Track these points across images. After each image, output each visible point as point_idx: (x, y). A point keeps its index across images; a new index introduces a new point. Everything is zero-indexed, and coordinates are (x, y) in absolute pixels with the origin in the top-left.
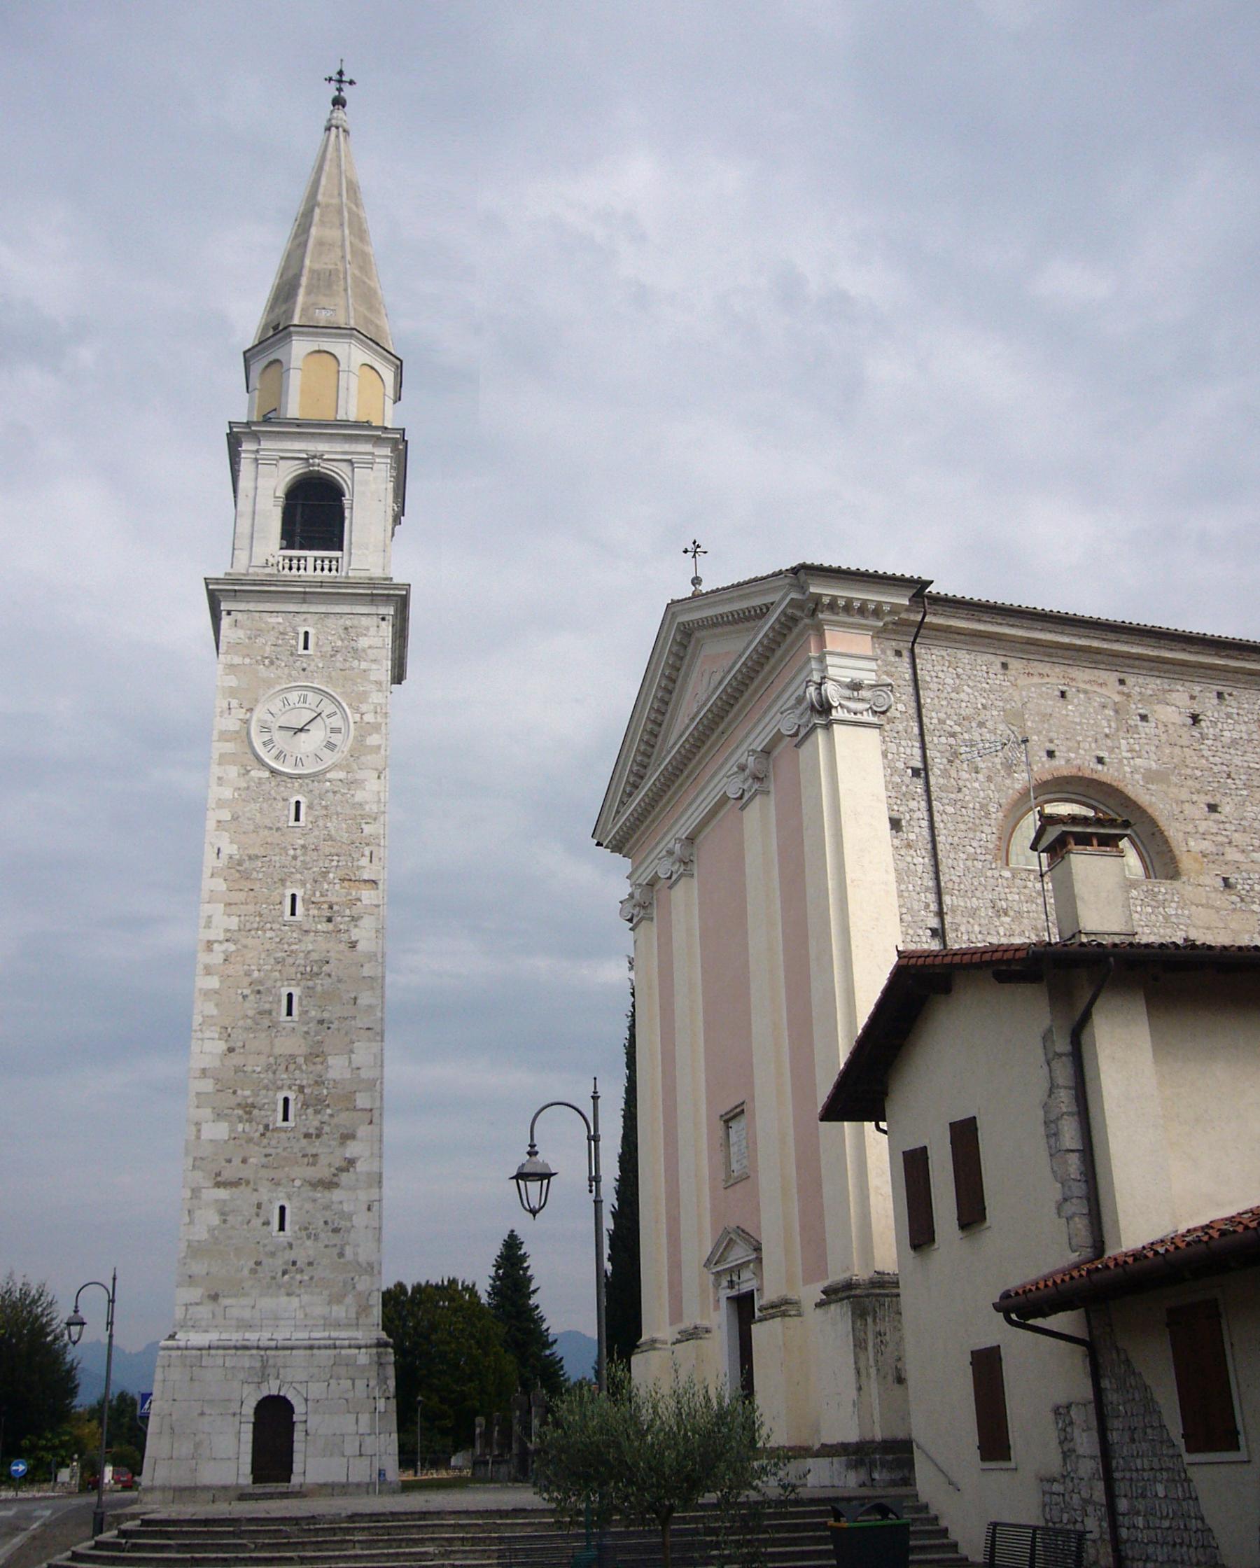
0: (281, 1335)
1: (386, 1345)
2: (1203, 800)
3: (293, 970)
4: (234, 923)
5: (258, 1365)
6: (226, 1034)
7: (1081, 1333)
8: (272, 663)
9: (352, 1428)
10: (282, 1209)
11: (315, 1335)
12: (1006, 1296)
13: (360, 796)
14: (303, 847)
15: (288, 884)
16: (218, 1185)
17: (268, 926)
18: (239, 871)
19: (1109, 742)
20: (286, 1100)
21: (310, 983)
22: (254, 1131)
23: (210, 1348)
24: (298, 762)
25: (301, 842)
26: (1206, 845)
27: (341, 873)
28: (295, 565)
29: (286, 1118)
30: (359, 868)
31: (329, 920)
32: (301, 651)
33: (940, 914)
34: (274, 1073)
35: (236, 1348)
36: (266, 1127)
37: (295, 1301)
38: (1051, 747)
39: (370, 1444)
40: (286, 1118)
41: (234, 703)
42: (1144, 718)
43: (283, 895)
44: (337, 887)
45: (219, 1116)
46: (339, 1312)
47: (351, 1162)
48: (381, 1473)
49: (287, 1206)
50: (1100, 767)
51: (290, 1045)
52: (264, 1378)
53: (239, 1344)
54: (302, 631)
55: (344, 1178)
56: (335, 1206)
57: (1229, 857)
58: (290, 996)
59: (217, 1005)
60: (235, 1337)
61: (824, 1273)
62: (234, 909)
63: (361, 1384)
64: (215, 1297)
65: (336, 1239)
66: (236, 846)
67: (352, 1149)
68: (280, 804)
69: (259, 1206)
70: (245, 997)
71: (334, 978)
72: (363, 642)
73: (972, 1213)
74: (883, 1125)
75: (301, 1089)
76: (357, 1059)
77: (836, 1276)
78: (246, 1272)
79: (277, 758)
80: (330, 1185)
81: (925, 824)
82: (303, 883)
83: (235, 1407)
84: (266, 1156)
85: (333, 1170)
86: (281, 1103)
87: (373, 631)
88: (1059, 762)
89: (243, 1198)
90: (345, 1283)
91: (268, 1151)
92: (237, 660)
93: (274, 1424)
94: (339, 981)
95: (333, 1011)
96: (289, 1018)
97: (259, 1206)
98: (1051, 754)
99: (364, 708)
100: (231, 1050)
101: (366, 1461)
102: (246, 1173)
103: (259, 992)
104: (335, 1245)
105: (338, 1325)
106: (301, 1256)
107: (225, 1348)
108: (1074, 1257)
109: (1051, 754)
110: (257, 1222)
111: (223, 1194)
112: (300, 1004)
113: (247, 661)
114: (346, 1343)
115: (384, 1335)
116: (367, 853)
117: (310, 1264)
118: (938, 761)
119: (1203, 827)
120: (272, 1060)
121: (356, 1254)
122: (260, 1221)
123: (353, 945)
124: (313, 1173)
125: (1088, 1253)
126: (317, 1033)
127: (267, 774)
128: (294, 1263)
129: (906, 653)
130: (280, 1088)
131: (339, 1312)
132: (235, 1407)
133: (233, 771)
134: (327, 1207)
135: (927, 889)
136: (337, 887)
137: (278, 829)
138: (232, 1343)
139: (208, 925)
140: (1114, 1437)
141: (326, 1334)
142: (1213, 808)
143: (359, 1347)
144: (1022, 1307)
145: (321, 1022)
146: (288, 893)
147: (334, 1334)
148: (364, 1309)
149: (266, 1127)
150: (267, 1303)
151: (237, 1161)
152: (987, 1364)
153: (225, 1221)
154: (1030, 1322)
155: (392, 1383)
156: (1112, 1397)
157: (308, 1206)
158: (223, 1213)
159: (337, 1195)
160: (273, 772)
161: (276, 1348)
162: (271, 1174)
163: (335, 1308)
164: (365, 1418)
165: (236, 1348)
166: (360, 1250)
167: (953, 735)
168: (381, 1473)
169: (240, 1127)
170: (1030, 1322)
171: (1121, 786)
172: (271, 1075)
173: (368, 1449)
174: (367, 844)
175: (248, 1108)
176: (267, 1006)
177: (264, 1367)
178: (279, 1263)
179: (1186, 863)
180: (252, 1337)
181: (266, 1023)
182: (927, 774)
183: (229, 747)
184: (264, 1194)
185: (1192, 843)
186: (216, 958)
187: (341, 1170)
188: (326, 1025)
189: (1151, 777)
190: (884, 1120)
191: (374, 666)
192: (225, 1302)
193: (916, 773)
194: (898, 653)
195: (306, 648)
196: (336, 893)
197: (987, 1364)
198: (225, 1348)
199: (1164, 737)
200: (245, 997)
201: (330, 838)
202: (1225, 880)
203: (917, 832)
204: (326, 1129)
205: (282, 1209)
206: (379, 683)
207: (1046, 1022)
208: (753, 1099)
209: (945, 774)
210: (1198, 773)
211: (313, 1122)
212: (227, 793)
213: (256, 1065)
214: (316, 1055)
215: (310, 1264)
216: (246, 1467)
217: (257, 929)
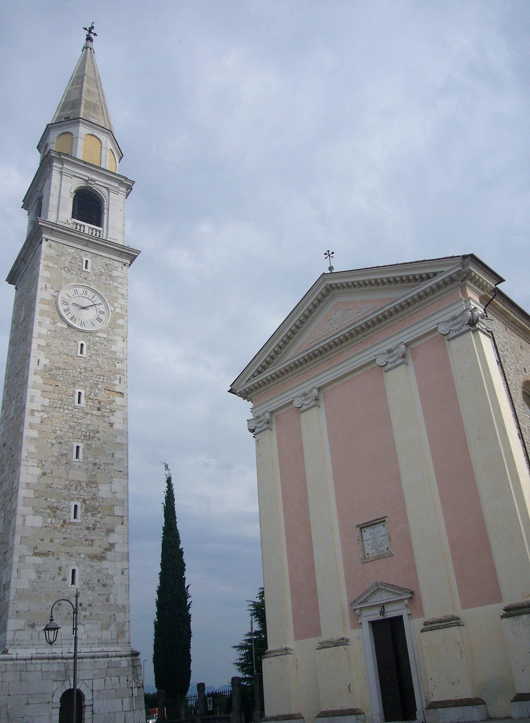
3: (80, 433)
4: (47, 402)
5: (63, 669)
6: (41, 464)
8: (69, 270)
10: (74, 571)
13: (114, 348)
14: (85, 368)
15: (77, 386)
16: (36, 554)
17: (66, 407)
18: (50, 374)
20: (76, 506)
21: (89, 442)
23: (32, 659)
25: (84, 365)
27: (105, 386)
30: (114, 385)
31: (99, 409)
34: (69, 490)
35: (48, 658)
36: (65, 521)
41: (49, 286)
45: (37, 512)
46: (107, 635)
47: (112, 546)
55: (109, 554)
56: (103, 571)
61: (501, 600)
63: (123, 679)
65: (104, 591)
67: (113, 538)
68: (73, 344)
69: (60, 569)
79: (71, 319)
80: (101, 558)
82: (85, 388)
83: (49, 698)
84: (64, 538)
87: (120, 269)
94: (105, 443)
96: (77, 460)
97: (60, 569)
100: (44, 474)
103: (60, 443)
104: (104, 595)
105: (106, 643)
110: (59, 579)
111: (38, 560)
113: (56, 266)
114: (114, 654)
117: (90, 605)
120: (68, 482)
121: (116, 600)
123: (111, 425)
124: (91, 550)
130: (73, 499)
131: (107, 635)
133: (47, 321)
134: (99, 571)
138: (46, 655)
139: (32, 401)
141: (100, 649)
143: (121, 657)
147: (105, 649)
149: (65, 521)
151: (47, 541)
153: (39, 577)
157: (89, 570)
159: (105, 564)
160: (69, 326)
162: (68, 550)
164: (127, 701)
165: (48, 658)
169: (49, 520)
174: (118, 373)
175: (54, 509)
176: (65, 452)
181: (64, 461)
183: (46, 308)
184: (63, 562)
191: (120, 286)
196: (103, 396)
200: (52, 445)
201: (98, 366)
204: (98, 525)
205: (74, 571)
211: (91, 521)
212: (44, 331)
214: (92, 482)
215: (90, 605)
217: (60, 408)
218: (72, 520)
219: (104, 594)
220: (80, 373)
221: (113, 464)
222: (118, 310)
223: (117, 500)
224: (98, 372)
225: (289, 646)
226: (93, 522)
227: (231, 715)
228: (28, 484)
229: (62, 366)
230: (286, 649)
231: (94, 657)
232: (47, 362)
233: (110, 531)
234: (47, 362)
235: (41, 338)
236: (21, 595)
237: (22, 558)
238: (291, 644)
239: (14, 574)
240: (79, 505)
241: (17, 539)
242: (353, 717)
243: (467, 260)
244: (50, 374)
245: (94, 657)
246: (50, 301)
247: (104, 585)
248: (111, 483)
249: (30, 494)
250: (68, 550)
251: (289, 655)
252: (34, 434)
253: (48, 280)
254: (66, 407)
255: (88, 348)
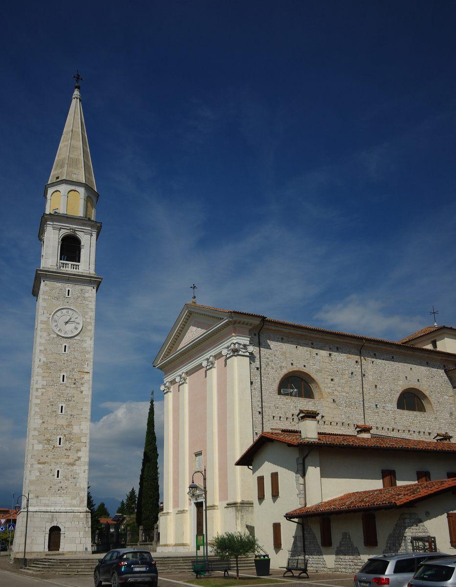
0: (57, 509)
1: (89, 512)
2: (330, 378)
3: (63, 398)
4: (45, 383)
5: (51, 517)
6: (42, 417)
7: (301, 522)
8: (58, 299)
9: (78, 536)
10: (58, 471)
11: (68, 509)
12: (287, 514)
13: (85, 345)
14: (67, 360)
15: (62, 372)
16: (39, 463)
17: (55, 385)
18: (47, 366)
19: (307, 361)
20: (60, 439)
21: (68, 403)
22: (50, 447)
23: (36, 512)
24: (65, 333)
25: (66, 359)
26: (330, 391)
27: (78, 369)
28: (64, 266)
29: (60, 444)
30: (84, 368)
31: (75, 384)
32: (67, 296)
33: (262, 408)
34: (57, 430)
35: (44, 512)
36: (54, 446)
37: (61, 499)
38: (292, 362)
39: (83, 541)
40: (60, 444)
41: (45, 312)
42: (317, 354)
43: (60, 375)
44: (77, 374)
45: (40, 442)
46: (75, 502)
47: (79, 458)
48: (86, 549)
49: (60, 471)
50: (304, 368)
51: (62, 422)
52: (52, 521)
53: (45, 511)
54: (67, 289)
55: (77, 462)
56: (74, 471)
57: (335, 394)
58: (62, 407)
59: (39, 408)
60: (44, 509)
61: (227, 499)
62: (45, 379)
63: (81, 523)
64: (37, 497)
65: (74, 481)
66: (45, 359)
67: (80, 454)
68: (59, 346)
69: (51, 470)
70: (48, 406)
71: (76, 402)
72: (87, 295)
73: (275, 495)
74: (250, 467)
75: (65, 435)
76: (82, 427)
77: (231, 501)
78: (47, 490)
79: (59, 331)
80: (73, 464)
81: (259, 383)
82: (67, 372)
83: (44, 529)
84: (54, 455)
85: (74, 460)
86: (58, 440)
87: (90, 292)
88: (294, 366)
89: (46, 467)
90: (77, 493)
91: (55, 454)
92: (46, 297)
93: (55, 533)
94: (77, 403)
95: (75, 412)
96: (61, 414)
97: (51, 470)
98: (292, 364)
99: (86, 317)
100: (43, 422)
101: (82, 545)
102: (47, 460)
103: (52, 405)
104: (74, 483)
105: (74, 506)
106: (63, 485)
107: (41, 512)
108: (300, 506)
109: (292, 364)
110: (51, 475)
111: (40, 466)
112: (65, 409)
113: (49, 298)
114: (77, 511)
115: (88, 509)
116: (87, 364)
117: (66, 488)
118: (263, 366)
119: (329, 385)
120: (56, 426)
121: (80, 485)
122: (51, 474)
123: (82, 392)
124: (67, 461)
125: (303, 506)
126: (70, 419)
127: (56, 336)
128: (61, 488)
129: (257, 335)
130: (58, 435)
131: (75, 502)
132: (44, 529)
133: (45, 334)
134: (72, 471)
135: (259, 401)
136: (77, 374)
137: (59, 354)
138: (43, 510)
139: (37, 383)
140: (306, 543)
141: (71, 508)
142: (332, 380)
143: (80, 513)
144: (289, 517)
145: (71, 415)
146: (62, 375)
147: (73, 508)
148: (82, 502)
149: (54, 446)
150: (53, 499)
151: (44, 457)
152: (277, 527)
153: (41, 474)
154: (291, 520)
155: (90, 523)
156: (306, 535)
157: (66, 470)
158: (40, 472)
159: (75, 467)
160: (58, 335)
161: (56, 512)
162: (56, 460)
163: (74, 501)
164: (82, 533)
165: (44, 512)
166: (81, 484)
167: (268, 358)
168: (86, 549)
169: (46, 446)
170: (291, 520)
171: (309, 373)
172: (55, 430)
173: (83, 542)
174: (87, 361)
175: (49, 440)
176: (55, 410)
177: (52, 517)
178: (57, 487)
179: (325, 395)
180: (49, 509)
181: (55, 415)
182: (261, 370)
183: (44, 326)
184: (53, 467)
185: (326, 390)
186: (39, 393)
187: (76, 460)
188: (73, 416)
189: (317, 371)
190: (251, 465)
191: (90, 303)
192: (40, 498)
193: (258, 369)
194: (255, 335)
195: (68, 295)
196: (77, 376)
197: (277, 527)
198: (41, 512)
199: (321, 360)
200: (48, 406)
201: (75, 358)
202: (334, 400)
203: (257, 385)
204: (72, 448)
205: (58, 471)
206: (92, 309)
207: (298, 456)
208: (206, 450)
209: (265, 369)
210: (329, 370)
211: (68, 445)
212: (43, 341)
213: (51, 427)
214: (70, 425)
215: (66, 488)
216: (47, 547)
217: (52, 385)
218: (58, 445)
219: (74, 483)
220: (64, 364)
221: (81, 414)
222: (88, 320)
223: (83, 434)
224: (74, 362)
225: (169, 511)
226: (69, 446)
227: (153, 543)
228: (35, 428)
229: (54, 361)
230: (168, 513)
231: (66, 512)
232: (45, 359)
233: (78, 450)
234: (45, 359)
235: (41, 346)
236: (32, 483)
237: (32, 465)
238: (217, 503)
239: (28, 473)
240: (62, 437)
241: (30, 456)
242: (183, 547)
243: (233, 313)
244: (47, 366)
245: (66, 512)
246: (46, 321)
247: (74, 478)
248: (80, 425)
249: (36, 433)
250: (56, 460)
251: (215, 510)
252: (38, 401)
253: (45, 308)
254: (55, 385)
255: (69, 348)
